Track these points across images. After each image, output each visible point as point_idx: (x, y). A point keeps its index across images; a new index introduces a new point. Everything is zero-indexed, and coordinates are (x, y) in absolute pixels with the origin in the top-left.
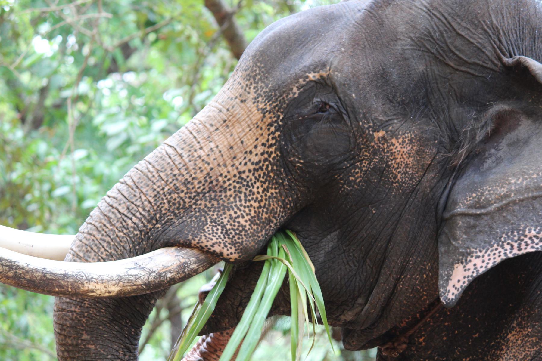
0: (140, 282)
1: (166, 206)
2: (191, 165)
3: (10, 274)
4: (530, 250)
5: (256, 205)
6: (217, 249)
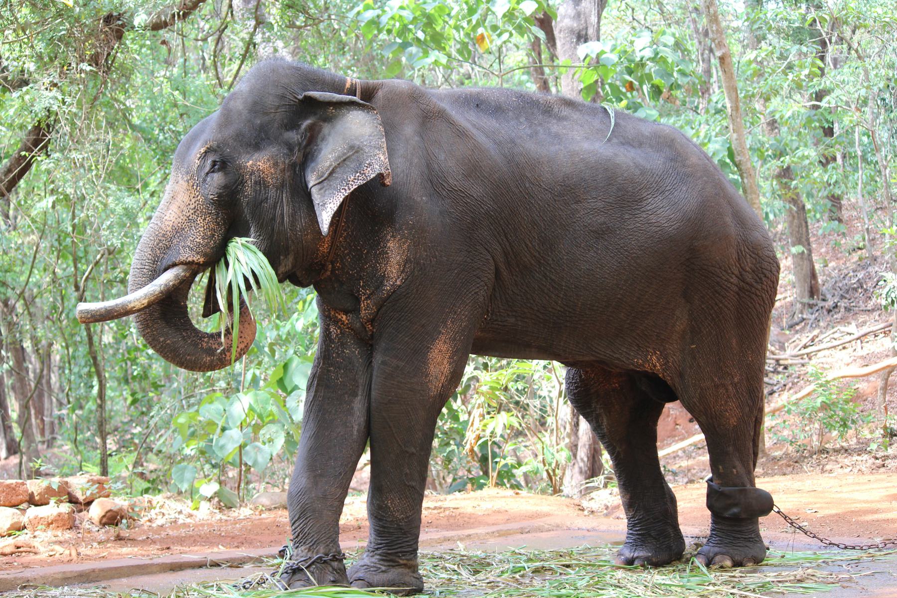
0: (157, 293)
1: (159, 252)
2: (163, 226)
3: (89, 316)
4: (355, 187)
5: (202, 229)
6: (190, 259)
